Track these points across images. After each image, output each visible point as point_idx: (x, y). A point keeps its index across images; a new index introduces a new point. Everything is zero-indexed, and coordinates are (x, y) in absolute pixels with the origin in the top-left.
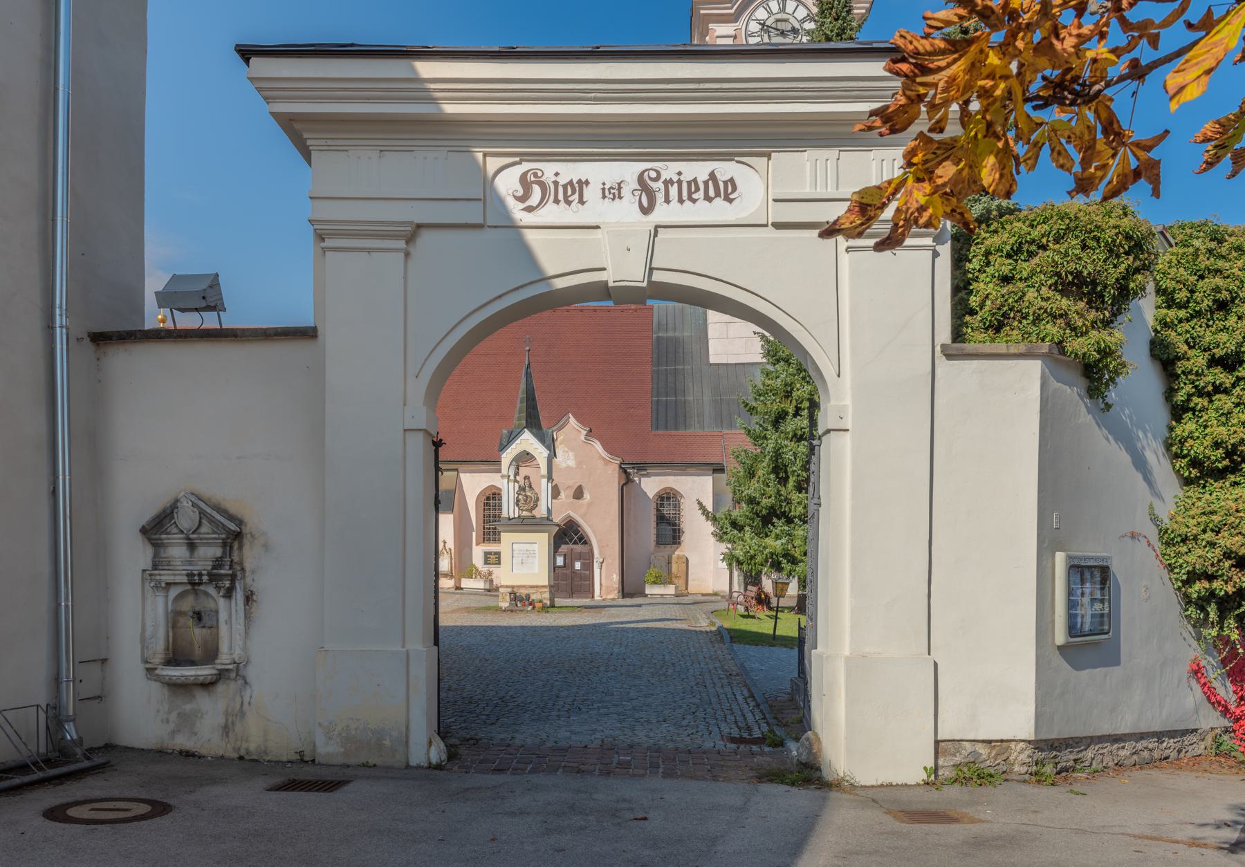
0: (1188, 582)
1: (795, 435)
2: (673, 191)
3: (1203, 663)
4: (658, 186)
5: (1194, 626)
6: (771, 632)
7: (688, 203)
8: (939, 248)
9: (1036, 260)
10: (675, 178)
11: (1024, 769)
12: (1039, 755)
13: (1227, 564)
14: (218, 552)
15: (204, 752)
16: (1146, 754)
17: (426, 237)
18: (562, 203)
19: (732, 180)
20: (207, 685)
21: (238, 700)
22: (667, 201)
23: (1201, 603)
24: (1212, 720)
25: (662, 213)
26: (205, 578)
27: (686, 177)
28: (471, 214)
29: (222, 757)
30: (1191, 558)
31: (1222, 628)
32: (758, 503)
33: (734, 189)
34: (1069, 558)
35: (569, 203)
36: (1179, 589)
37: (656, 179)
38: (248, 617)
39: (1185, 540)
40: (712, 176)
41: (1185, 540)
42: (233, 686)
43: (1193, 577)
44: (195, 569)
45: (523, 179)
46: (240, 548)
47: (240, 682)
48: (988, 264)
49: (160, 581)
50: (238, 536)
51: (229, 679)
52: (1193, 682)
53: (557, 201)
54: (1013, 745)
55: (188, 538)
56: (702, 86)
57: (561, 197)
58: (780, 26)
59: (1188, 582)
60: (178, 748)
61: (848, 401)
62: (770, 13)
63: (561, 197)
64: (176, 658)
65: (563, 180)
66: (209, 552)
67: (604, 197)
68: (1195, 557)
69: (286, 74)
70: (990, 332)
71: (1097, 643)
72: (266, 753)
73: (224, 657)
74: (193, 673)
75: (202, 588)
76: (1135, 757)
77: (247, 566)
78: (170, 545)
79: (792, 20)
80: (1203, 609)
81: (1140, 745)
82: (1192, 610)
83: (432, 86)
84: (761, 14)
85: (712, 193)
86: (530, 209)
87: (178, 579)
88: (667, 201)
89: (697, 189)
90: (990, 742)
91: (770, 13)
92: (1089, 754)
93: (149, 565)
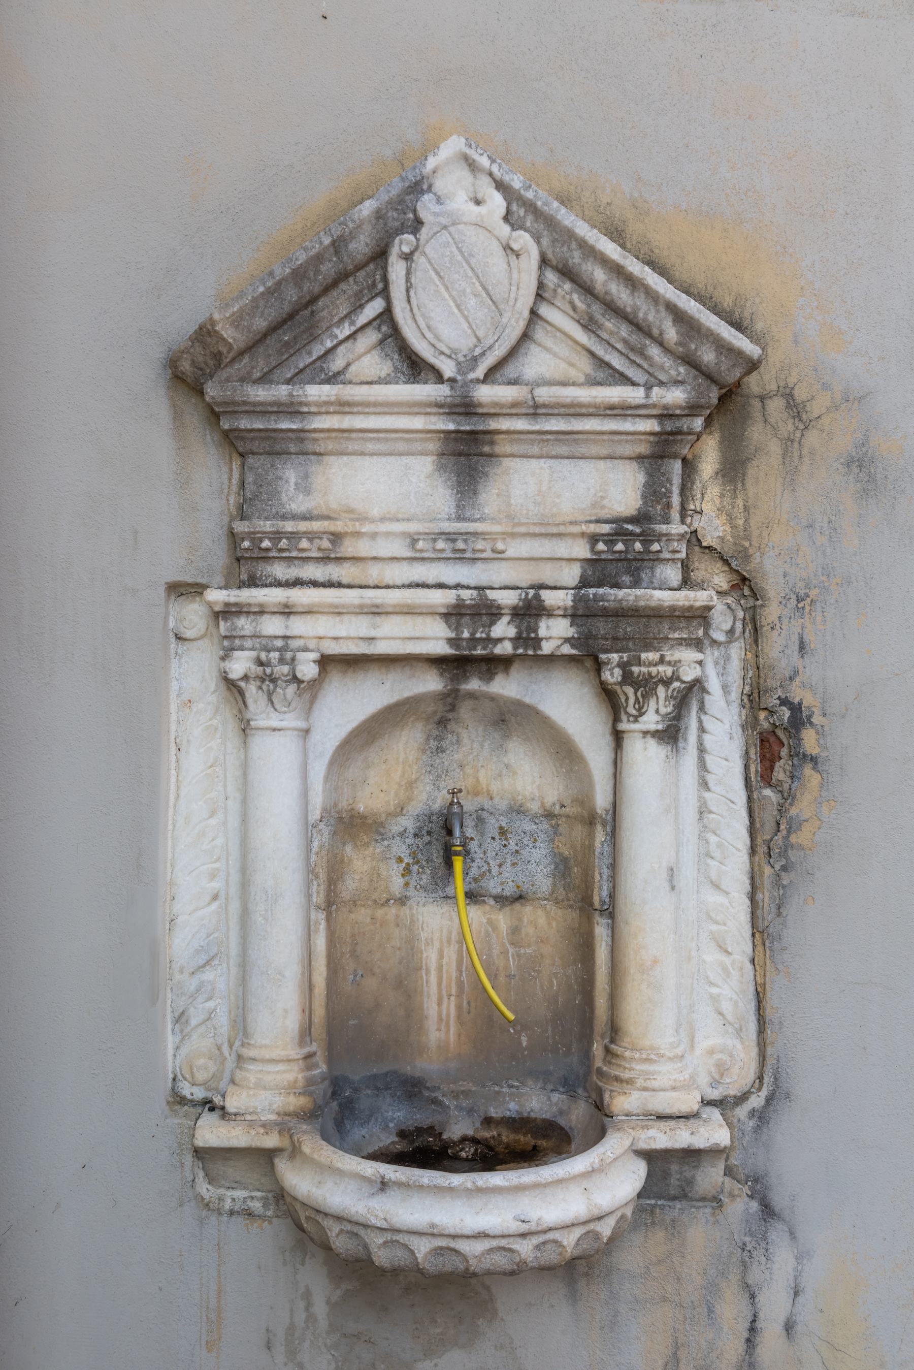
14: (620, 489)
21: (732, 1311)
26: (555, 632)
38: (773, 848)
44: (501, 580)
49: (286, 647)
55: (464, 407)
56: (386, 410)
66: (558, 499)
73: (665, 1073)
75: (506, 687)
87: (393, 635)
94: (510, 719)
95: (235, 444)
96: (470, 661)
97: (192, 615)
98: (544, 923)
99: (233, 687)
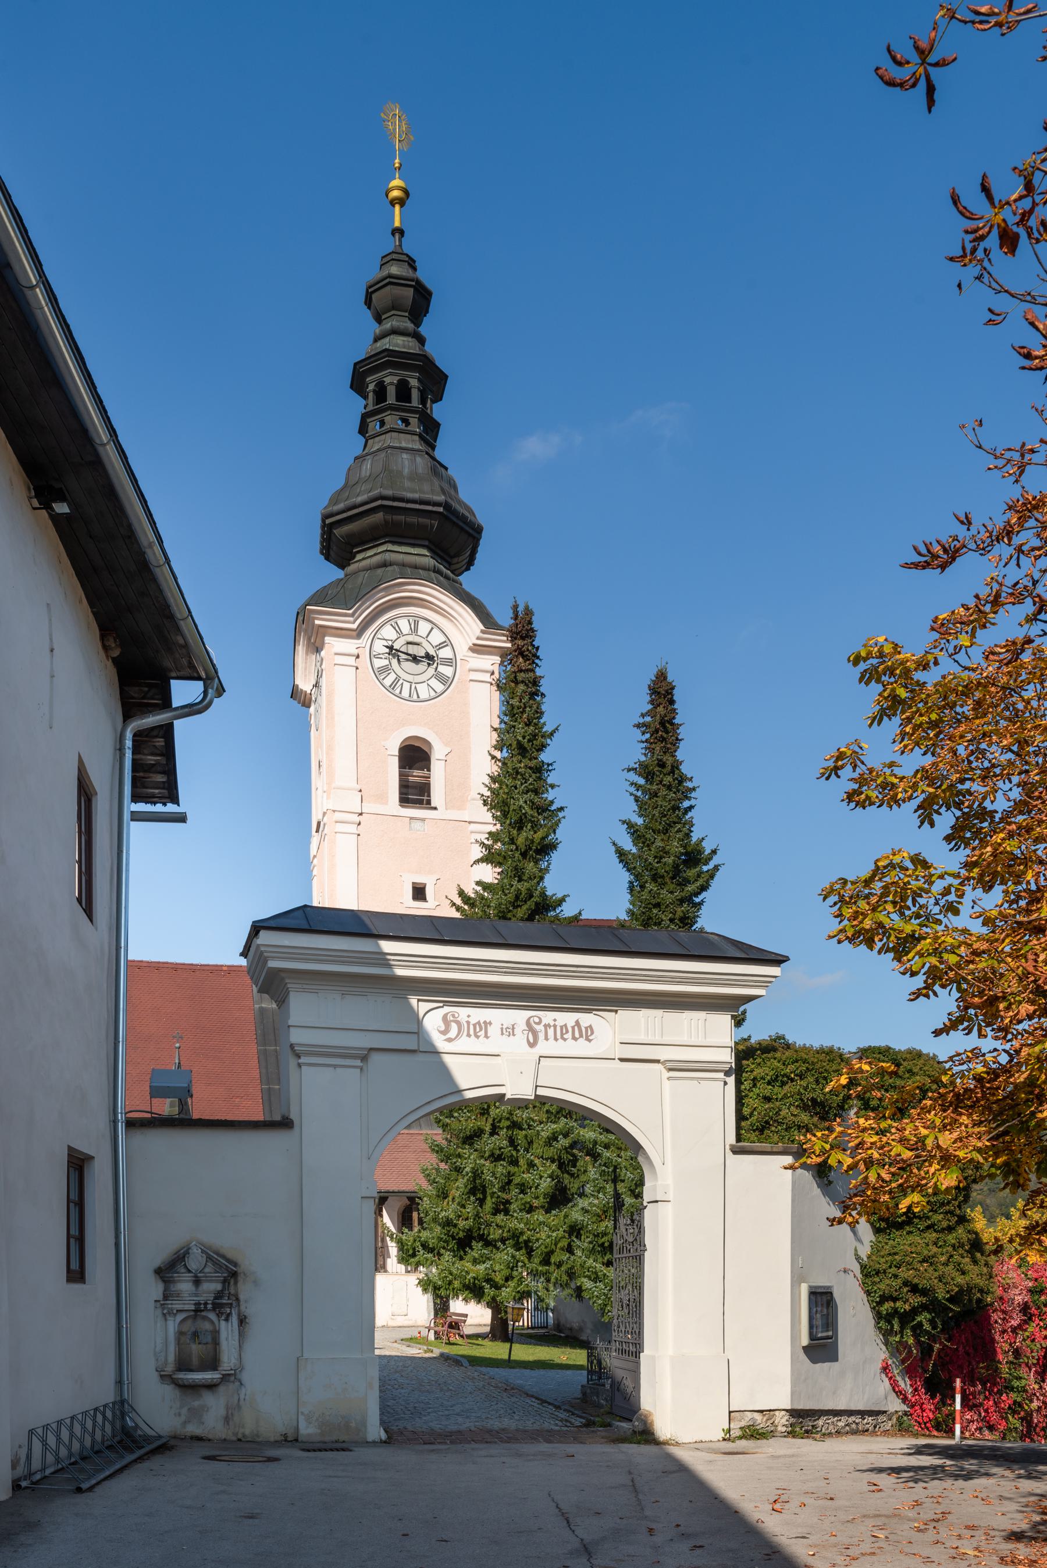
0: (880, 1303)
1: (492, 1155)
2: (551, 1031)
3: (890, 1362)
4: (540, 1028)
5: (883, 1335)
6: (506, 1357)
7: (560, 1041)
8: (728, 1079)
9: (786, 1087)
10: (552, 1023)
11: (784, 1429)
12: (792, 1420)
13: (905, 1290)
14: (219, 1287)
15: (210, 1436)
16: (854, 1426)
17: (375, 1057)
18: (473, 1037)
19: (590, 1026)
20: (211, 1387)
21: (236, 1398)
22: (547, 1039)
23: (888, 1318)
24: (896, 1405)
25: (545, 1047)
26: (209, 1306)
27: (559, 1023)
28: (410, 1043)
29: (225, 1440)
30: (882, 1286)
31: (902, 1337)
32: (455, 1226)
33: (592, 1033)
34: (810, 1287)
35: (478, 1037)
36: (874, 1308)
37: (539, 1023)
38: (242, 1334)
39: (878, 1273)
40: (577, 1023)
41: (878, 1273)
42: (232, 1387)
43: (884, 1299)
44: (202, 1299)
45: (445, 1018)
46: (236, 1283)
47: (237, 1383)
48: (755, 1086)
49: (172, 1309)
50: (234, 1275)
51: (229, 1381)
52: (883, 1376)
53: (469, 1035)
54: (777, 1413)
55: (196, 1276)
57: (472, 1032)
58: (412, 650)
59: (880, 1303)
60: (189, 1434)
61: (670, 1181)
62: (399, 632)
63: (472, 1032)
64: (183, 1365)
65: (473, 1021)
67: (502, 1034)
68: (884, 1285)
69: (287, 943)
70: (757, 1133)
71: (824, 1346)
72: (258, 1436)
74: (210, 1376)
75: (203, 1314)
76: (847, 1428)
77: (242, 1297)
78: (179, 1281)
79: (425, 644)
80: (890, 1322)
81: (851, 1419)
82: (882, 1324)
83: (389, 957)
84: (388, 632)
85: (577, 1035)
86: (450, 1040)
87: (187, 1307)
88: (547, 1039)
89: (567, 1032)
90: (761, 1411)
91: (399, 632)
92: (820, 1422)
93: (161, 1297)
94: (205, 1318)
95: (164, 1281)
96: (198, 1310)
97: (158, 1304)
98: (210, 1346)
99: (164, 1315)
